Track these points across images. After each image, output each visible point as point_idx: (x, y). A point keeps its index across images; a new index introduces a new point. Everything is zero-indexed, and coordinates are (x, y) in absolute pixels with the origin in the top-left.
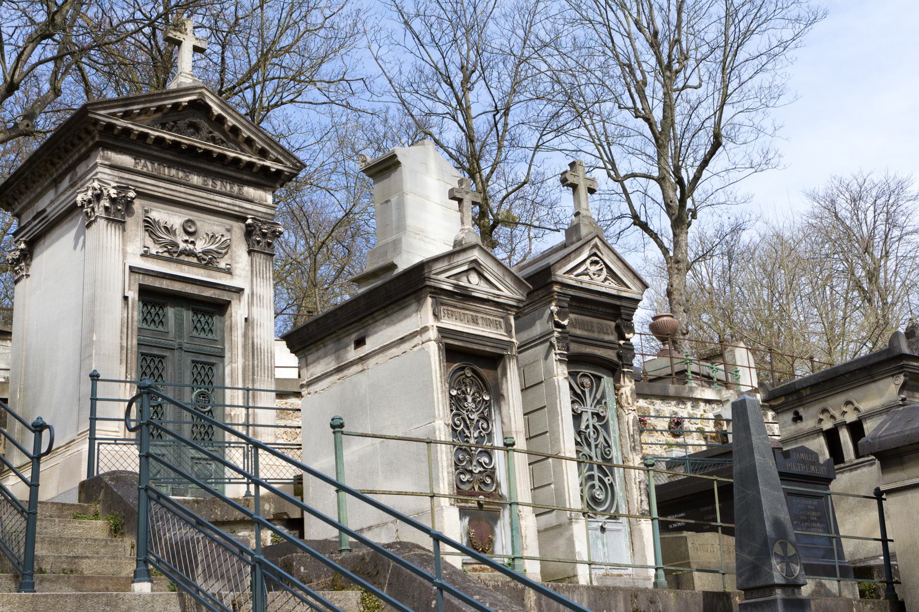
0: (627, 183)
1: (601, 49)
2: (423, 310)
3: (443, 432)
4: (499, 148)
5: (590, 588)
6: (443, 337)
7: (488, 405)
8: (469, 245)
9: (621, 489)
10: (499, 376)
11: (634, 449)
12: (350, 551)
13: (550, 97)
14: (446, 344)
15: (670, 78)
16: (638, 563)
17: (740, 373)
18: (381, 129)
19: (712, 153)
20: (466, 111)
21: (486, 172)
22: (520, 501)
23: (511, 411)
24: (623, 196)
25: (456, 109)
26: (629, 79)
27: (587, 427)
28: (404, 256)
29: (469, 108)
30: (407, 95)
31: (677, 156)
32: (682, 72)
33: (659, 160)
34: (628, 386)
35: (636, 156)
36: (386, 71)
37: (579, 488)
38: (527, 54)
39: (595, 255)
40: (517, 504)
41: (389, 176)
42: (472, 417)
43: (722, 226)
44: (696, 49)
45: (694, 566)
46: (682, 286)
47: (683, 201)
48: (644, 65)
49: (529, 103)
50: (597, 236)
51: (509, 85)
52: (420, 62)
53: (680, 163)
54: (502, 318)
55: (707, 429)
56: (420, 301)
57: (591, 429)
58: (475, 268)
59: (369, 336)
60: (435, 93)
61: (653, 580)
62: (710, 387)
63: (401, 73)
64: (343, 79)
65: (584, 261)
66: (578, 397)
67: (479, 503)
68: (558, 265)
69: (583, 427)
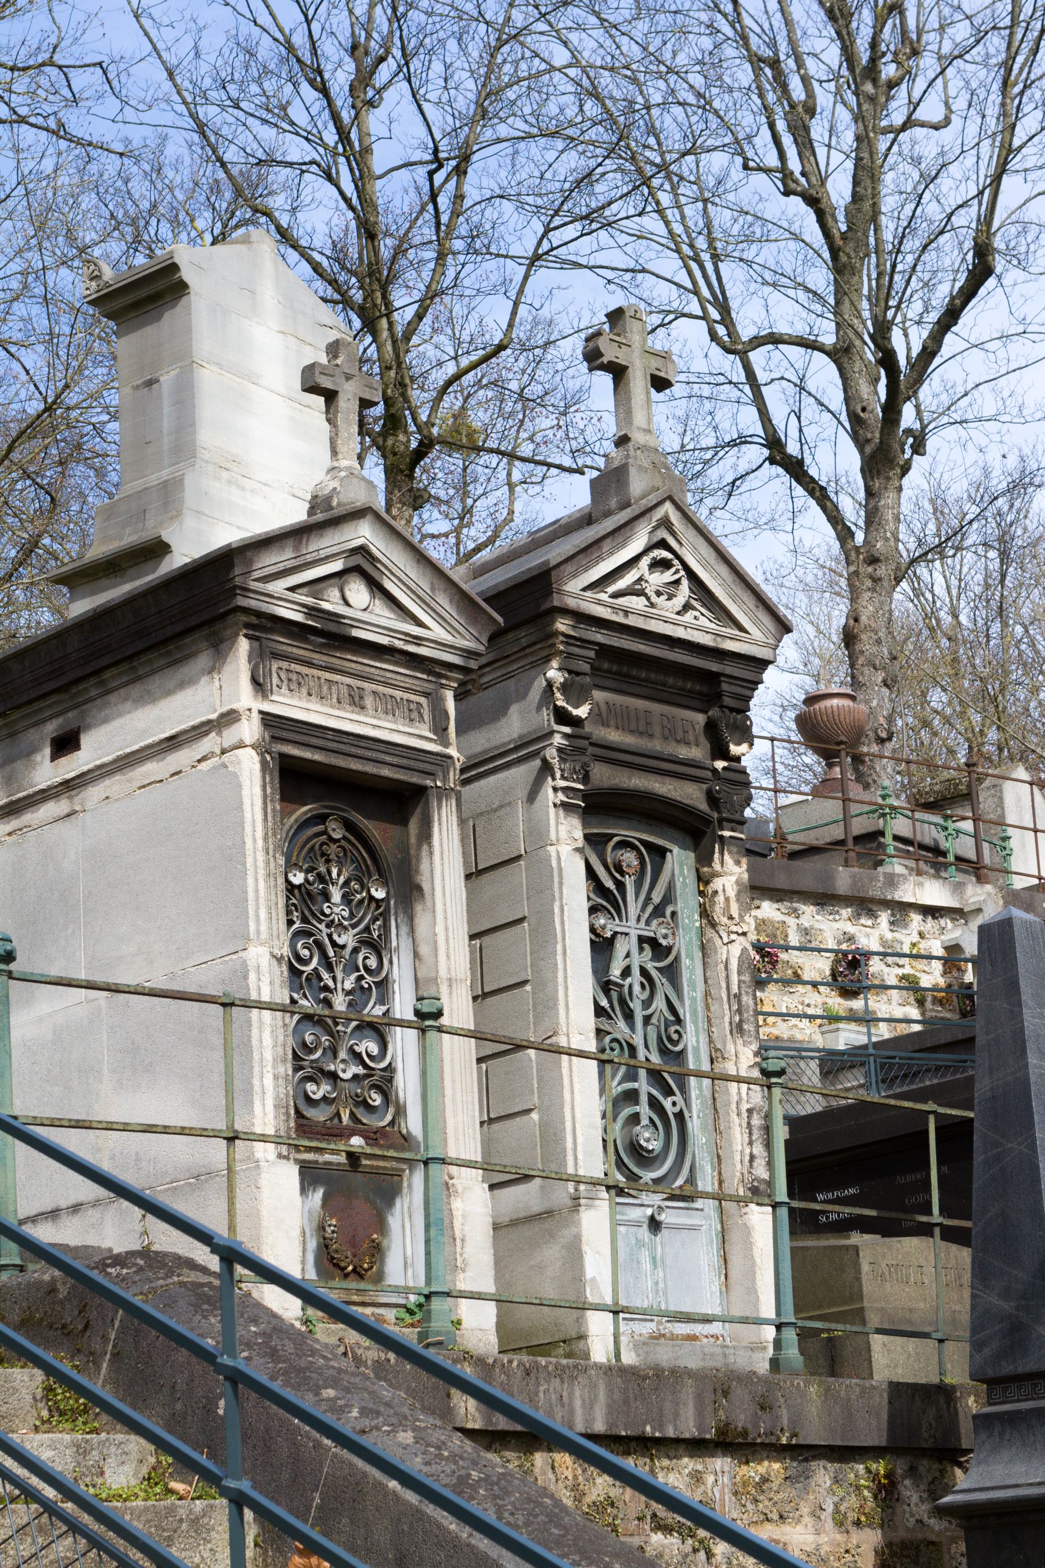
0: (756, 357)
1: (704, 17)
2: (228, 669)
3: (267, 982)
4: (441, 258)
5: (615, 1371)
6: (273, 738)
7: (381, 910)
8: (349, 508)
9: (704, 1127)
10: (413, 840)
11: (738, 1029)
12: (22, 1269)
13: (570, 132)
14: (282, 755)
15: (872, 99)
16: (737, 1312)
17: (1013, 843)
18: (139, 187)
19: (969, 292)
20: (360, 160)
21: (404, 316)
22: (452, 1153)
23: (440, 929)
24: (747, 389)
25: (336, 154)
26: (771, 97)
27: (626, 972)
28: (189, 522)
29: (366, 150)
30: (213, 110)
31: (882, 296)
32: (904, 86)
33: (838, 302)
34: (731, 874)
35: (782, 291)
36: (160, 46)
37: (599, 1122)
38: (518, 18)
39: (663, 544)
40: (443, 1161)
41: (158, 318)
42: (340, 941)
43: (987, 474)
44: (942, 29)
45: (874, 1320)
46: (882, 622)
47: (892, 410)
48: (810, 63)
49: (522, 145)
50: (670, 498)
51: (472, 96)
52: (247, 28)
53: (890, 314)
54: (426, 695)
55: (926, 982)
56: (220, 648)
57: (636, 976)
58: (362, 566)
59: (88, 727)
60: (284, 108)
61: (770, 1352)
62: (937, 876)
63: (197, 55)
64: (50, 62)
65: (635, 560)
66: (605, 898)
67: (350, 1155)
68: (569, 568)
69: (615, 972)
